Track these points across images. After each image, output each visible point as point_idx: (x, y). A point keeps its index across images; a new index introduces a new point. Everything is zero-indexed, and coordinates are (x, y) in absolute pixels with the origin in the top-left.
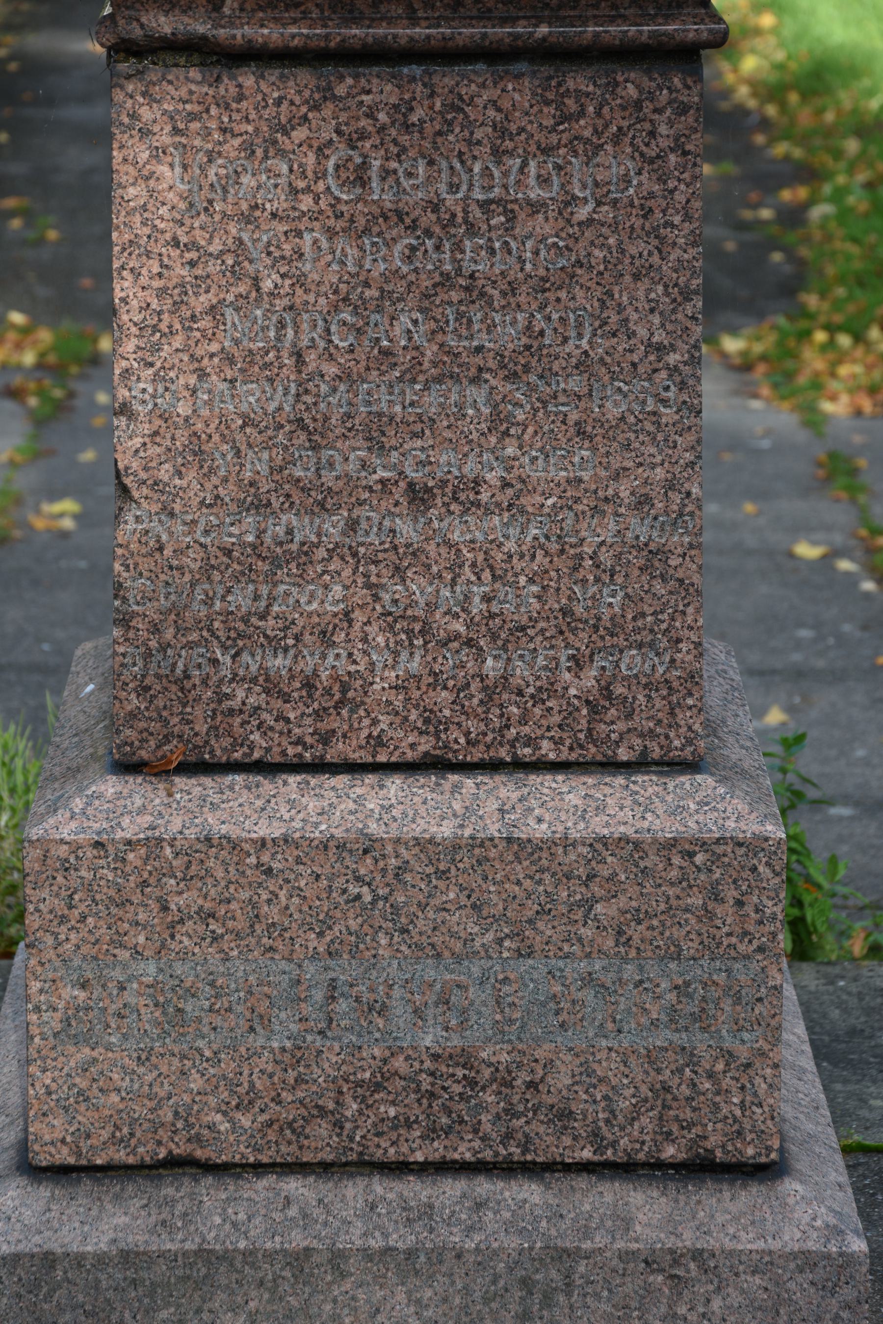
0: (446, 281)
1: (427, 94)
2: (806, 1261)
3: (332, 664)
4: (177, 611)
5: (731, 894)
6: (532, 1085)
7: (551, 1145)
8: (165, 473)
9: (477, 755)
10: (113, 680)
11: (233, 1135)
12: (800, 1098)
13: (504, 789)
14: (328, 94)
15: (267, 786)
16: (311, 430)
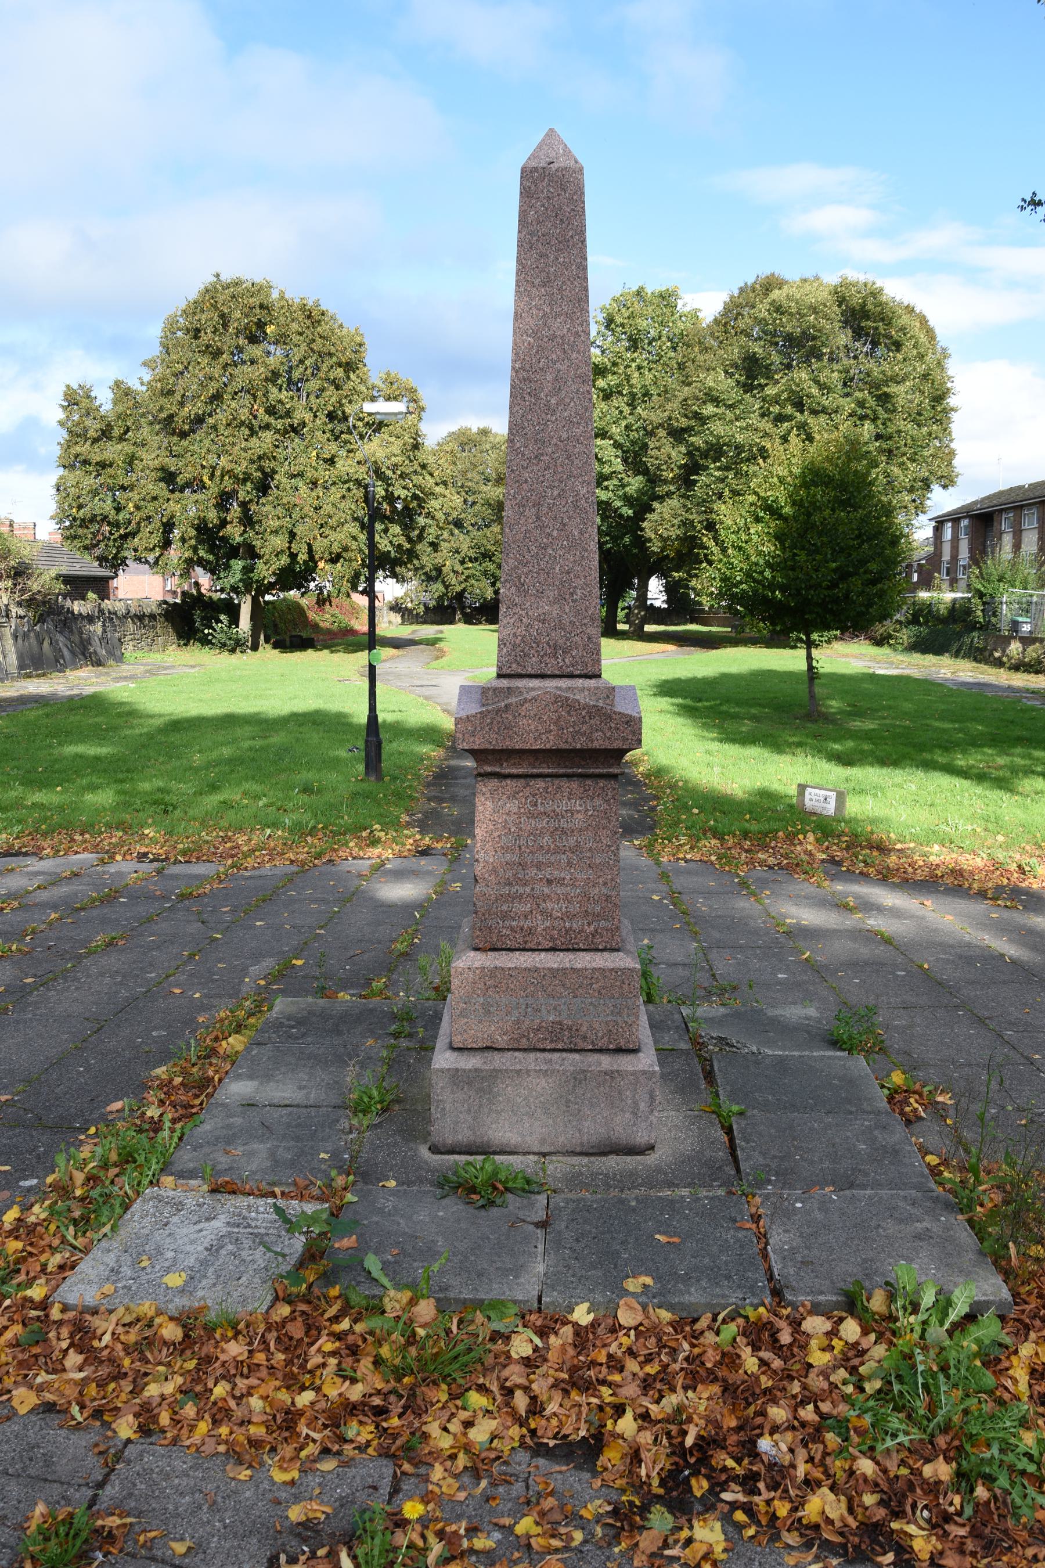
1: (552, 785)
2: (644, 1072)
3: (527, 924)
4: (489, 910)
7: (581, 1045)
10: (473, 928)
11: (502, 1041)
12: (644, 1033)
13: (571, 956)
15: (511, 954)
16: (523, 866)
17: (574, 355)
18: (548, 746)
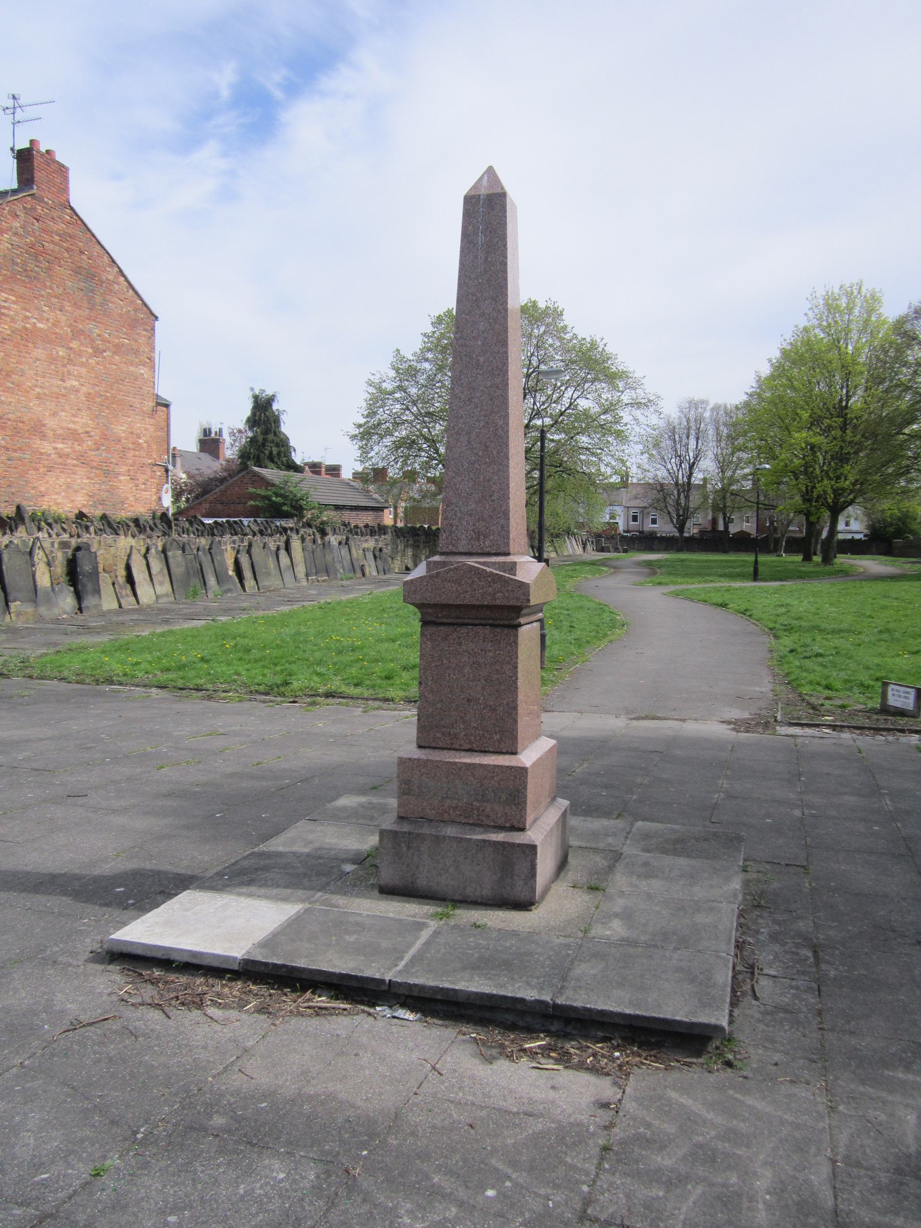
0: (474, 663)
7: (486, 821)
11: (431, 814)
17: (497, 326)
18: (465, 603)
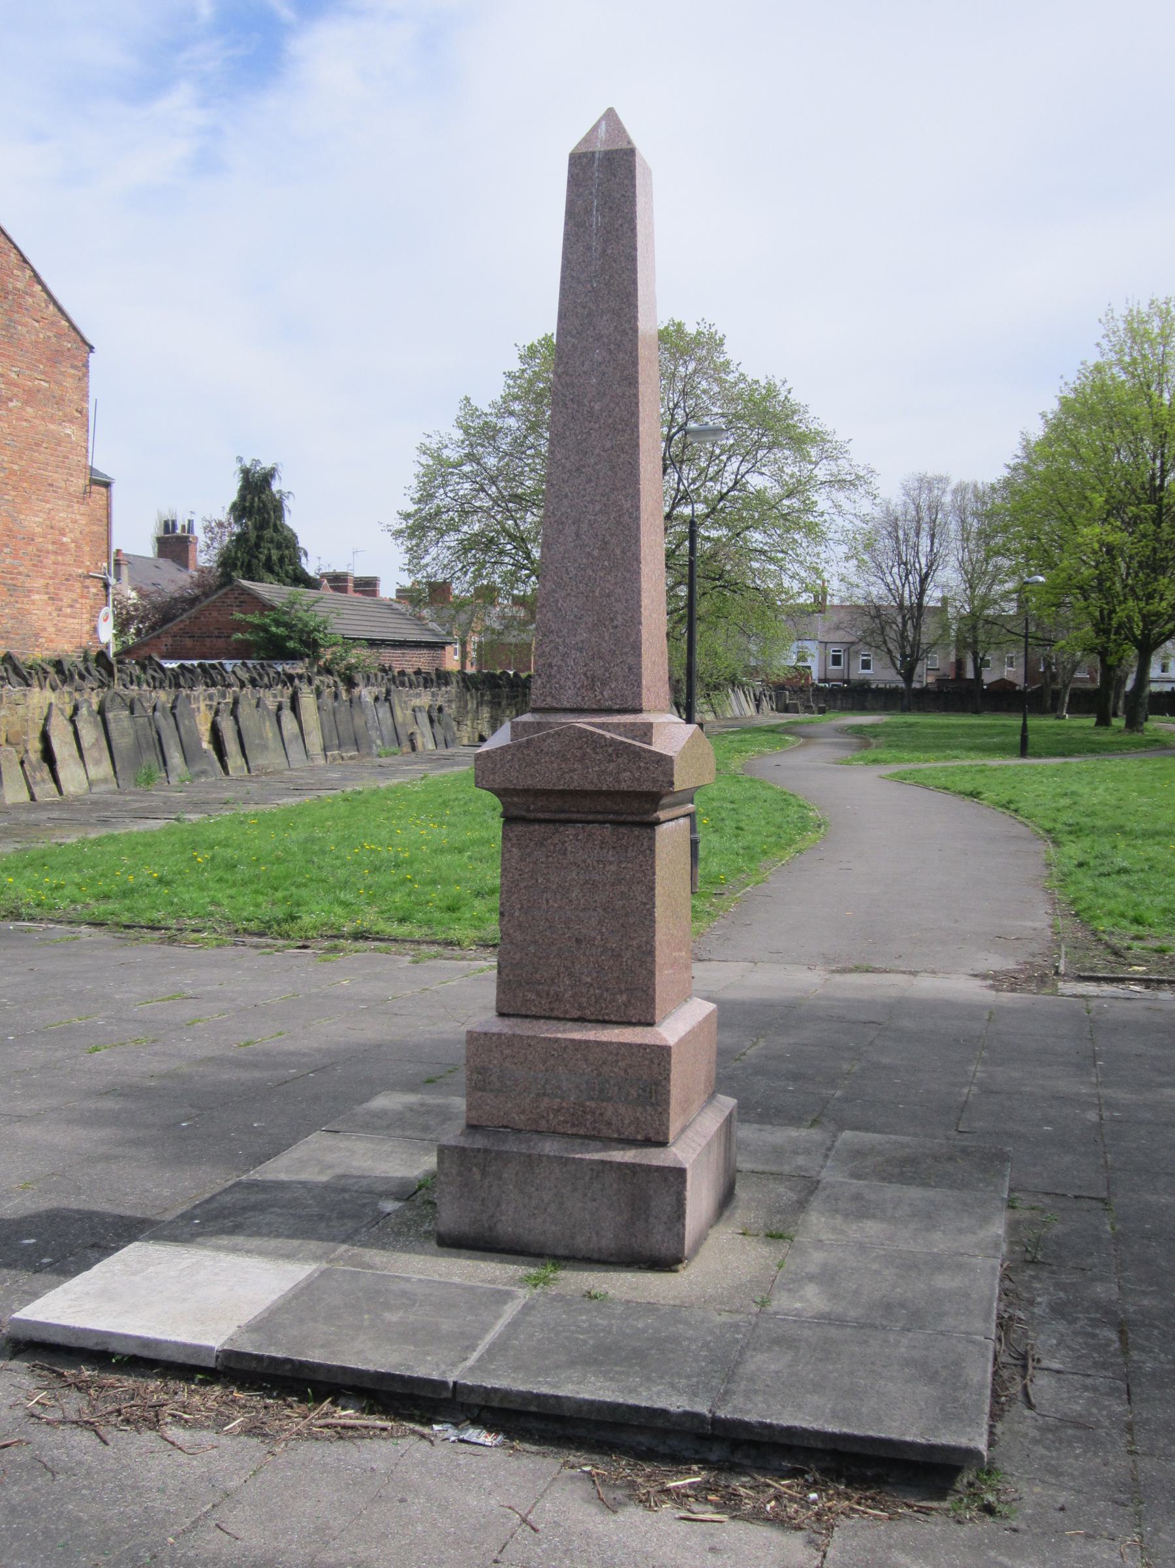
5: (656, 1061)
6: (601, 1114)
7: (606, 1132)
8: (511, 931)
9: (593, 1017)
13: (527, 1023)
14: (557, 831)
18: (572, 787)
